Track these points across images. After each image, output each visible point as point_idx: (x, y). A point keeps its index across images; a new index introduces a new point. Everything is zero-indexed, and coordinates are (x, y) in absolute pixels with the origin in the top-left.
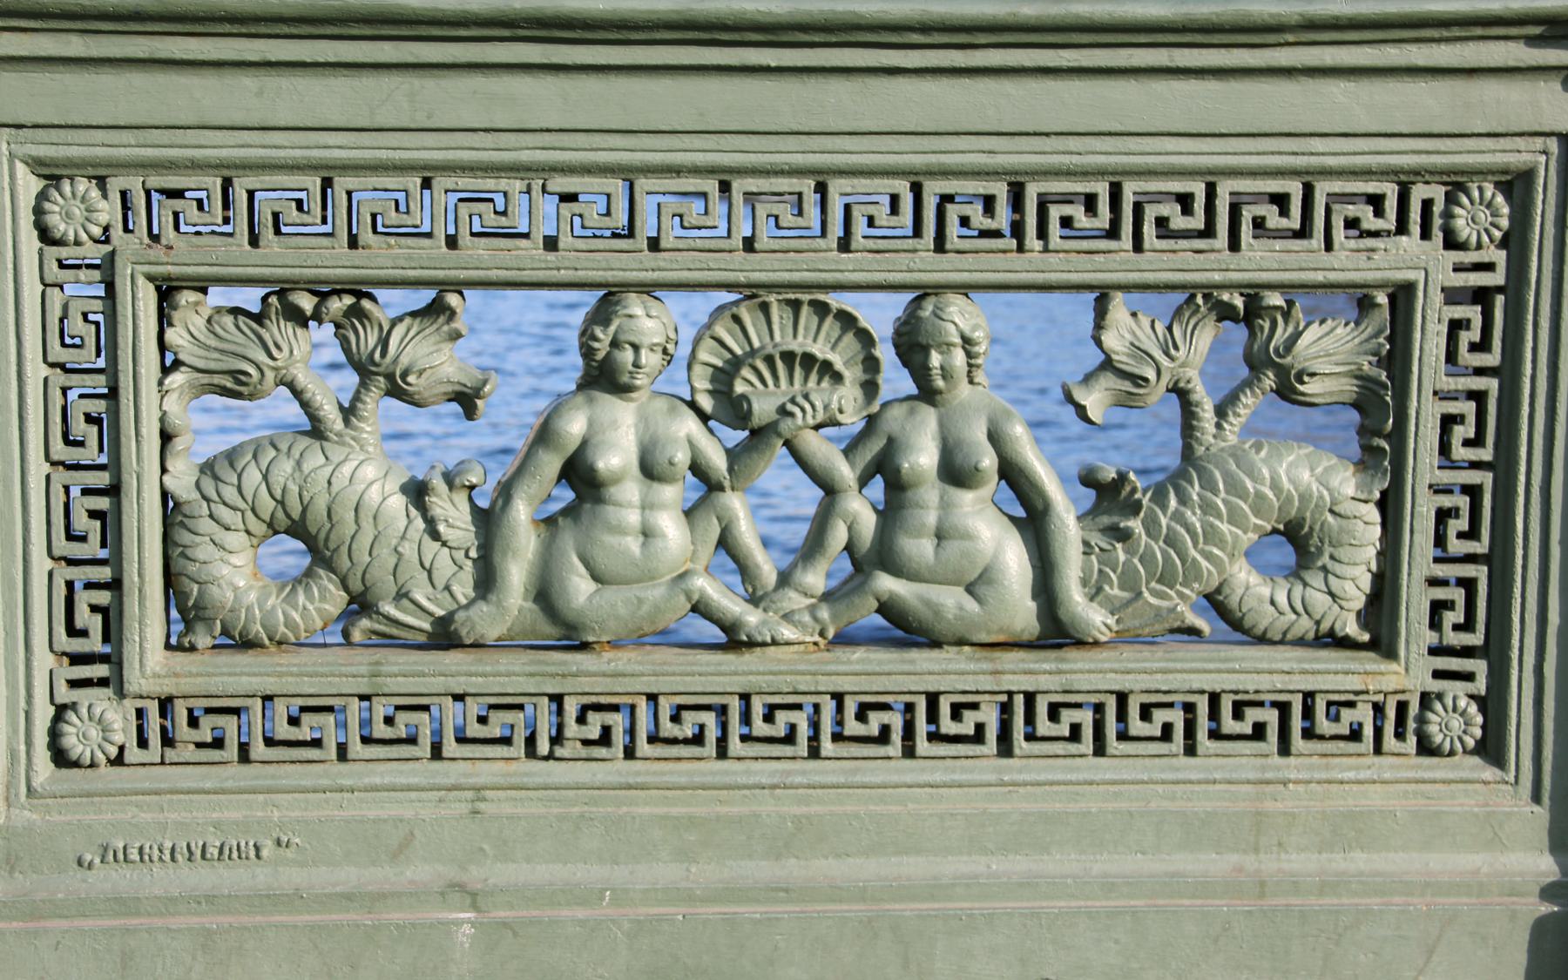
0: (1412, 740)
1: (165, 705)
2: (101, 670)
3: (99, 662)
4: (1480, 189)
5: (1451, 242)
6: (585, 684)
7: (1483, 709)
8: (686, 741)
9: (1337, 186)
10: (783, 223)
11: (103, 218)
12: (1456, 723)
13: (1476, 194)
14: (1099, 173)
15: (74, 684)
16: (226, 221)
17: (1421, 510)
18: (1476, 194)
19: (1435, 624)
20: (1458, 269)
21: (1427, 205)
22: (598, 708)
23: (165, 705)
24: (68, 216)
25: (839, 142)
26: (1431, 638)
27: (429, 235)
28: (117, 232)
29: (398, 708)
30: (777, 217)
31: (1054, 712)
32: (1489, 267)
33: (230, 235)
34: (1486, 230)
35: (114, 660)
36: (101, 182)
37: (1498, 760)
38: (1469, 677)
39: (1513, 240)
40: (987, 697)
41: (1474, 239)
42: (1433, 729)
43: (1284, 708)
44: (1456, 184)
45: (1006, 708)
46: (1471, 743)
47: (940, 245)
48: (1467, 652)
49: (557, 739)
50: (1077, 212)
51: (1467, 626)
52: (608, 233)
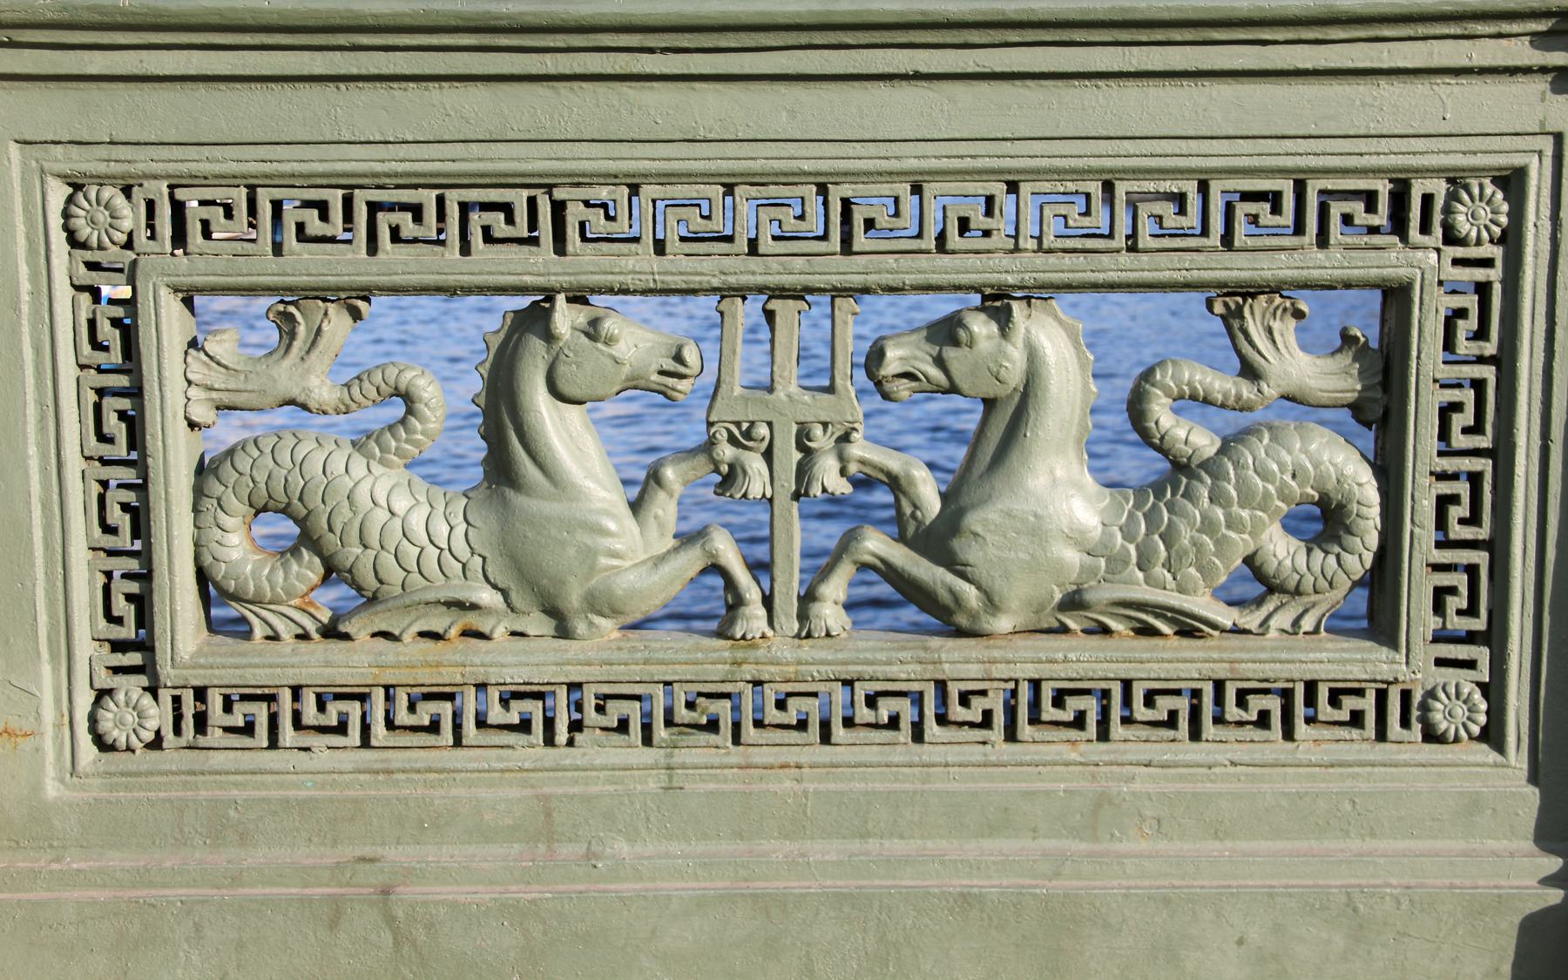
0: (1417, 727)
1: (200, 694)
2: (134, 658)
3: (138, 649)
4: (1481, 187)
5: (1451, 238)
6: (1060, 670)
7: (1485, 695)
8: (972, 725)
9: (1135, 186)
10: (1071, 223)
11: (127, 225)
12: (1460, 711)
13: (1476, 191)
14: (1282, 172)
15: (116, 670)
16: (440, 231)
17: (1421, 496)
18: (1476, 191)
19: (1439, 608)
20: (1457, 262)
21: (1428, 199)
22: (428, 697)
23: (200, 694)
24: (93, 222)
25: (1020, 148)
26: (1434, 622)
27: (636, 240)
28: (142, 236)
29: (700, 694)
30: (1161, 217)
31: (1242, 698)
32: (1487, 263)
33: (253, 241)
34: (1486, 227)
35: (145, 646)
36: (127, 191)
37: (1500, 747)
38: (1470, 664)
39: (1510, 238)
40: (996, 684)
41: (1474, 234)
42: (1437, 717)
43: (1287, 695)
44: (1456, 181)
45: (1382, 696)
46: (1476, 730)
47: (1323, 240)
48: (1471, 638)
49: (576, 726)
50: (1357, 208)
51: (1471, 611)
52: (660, 236)
